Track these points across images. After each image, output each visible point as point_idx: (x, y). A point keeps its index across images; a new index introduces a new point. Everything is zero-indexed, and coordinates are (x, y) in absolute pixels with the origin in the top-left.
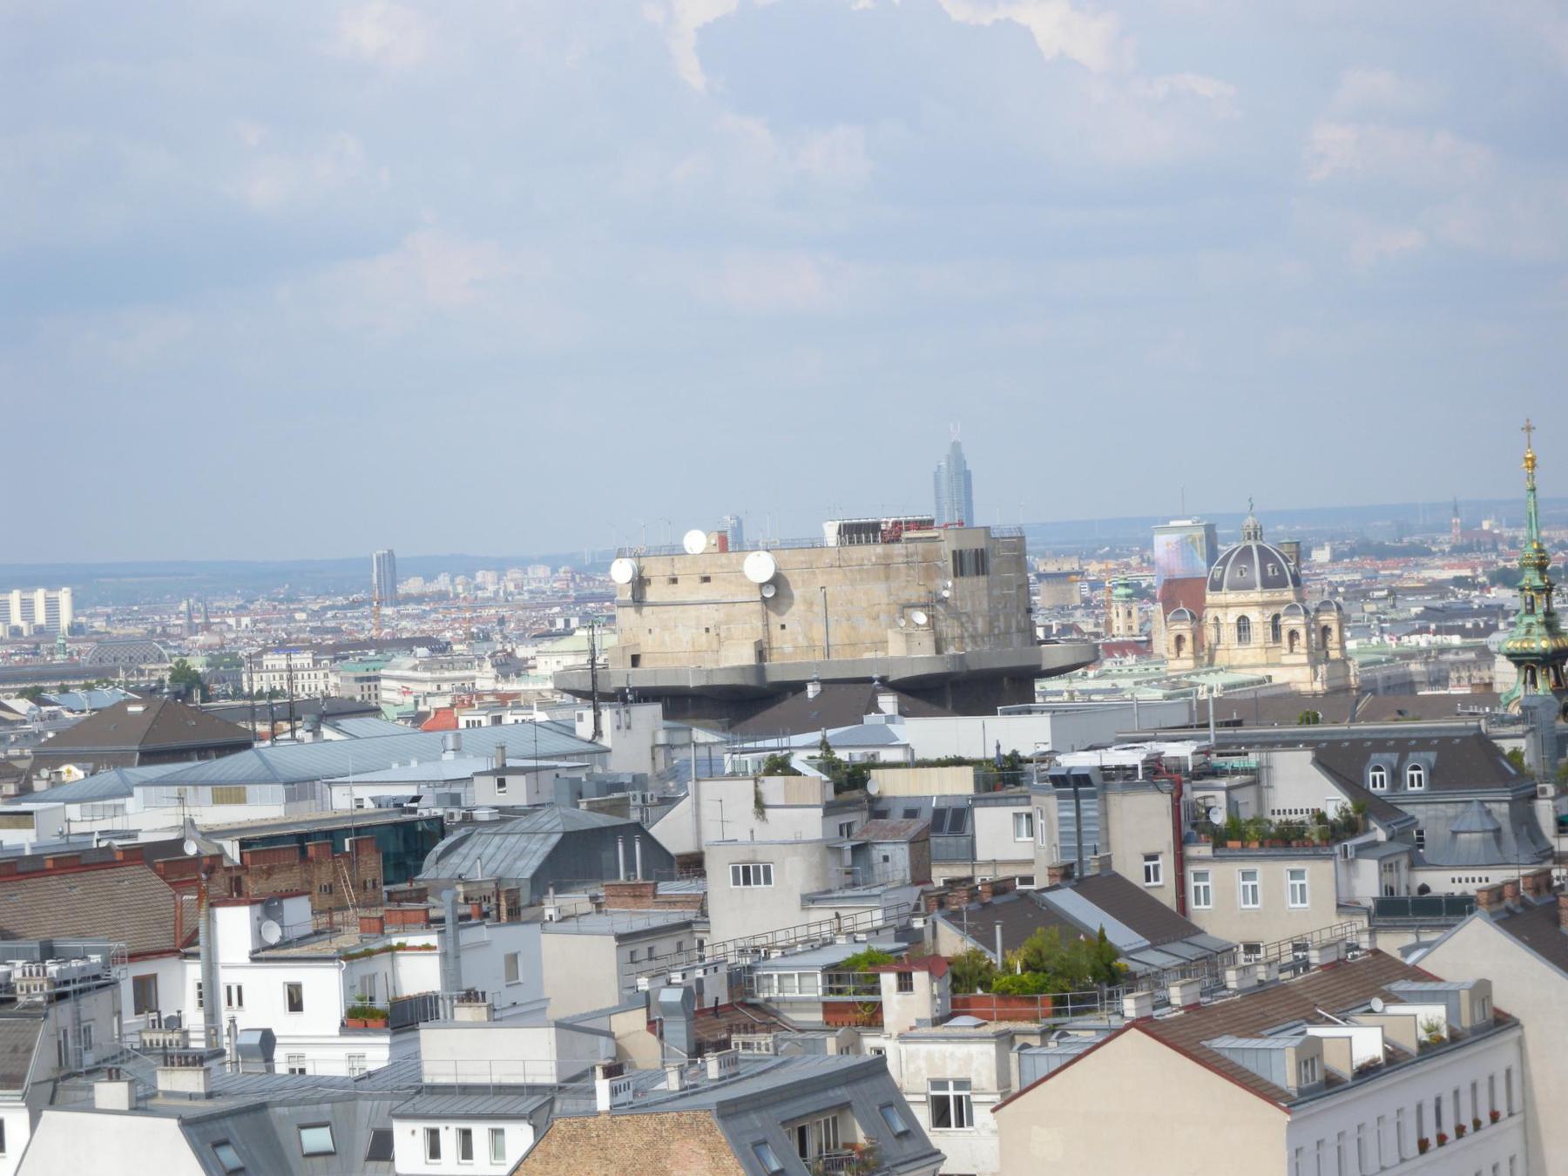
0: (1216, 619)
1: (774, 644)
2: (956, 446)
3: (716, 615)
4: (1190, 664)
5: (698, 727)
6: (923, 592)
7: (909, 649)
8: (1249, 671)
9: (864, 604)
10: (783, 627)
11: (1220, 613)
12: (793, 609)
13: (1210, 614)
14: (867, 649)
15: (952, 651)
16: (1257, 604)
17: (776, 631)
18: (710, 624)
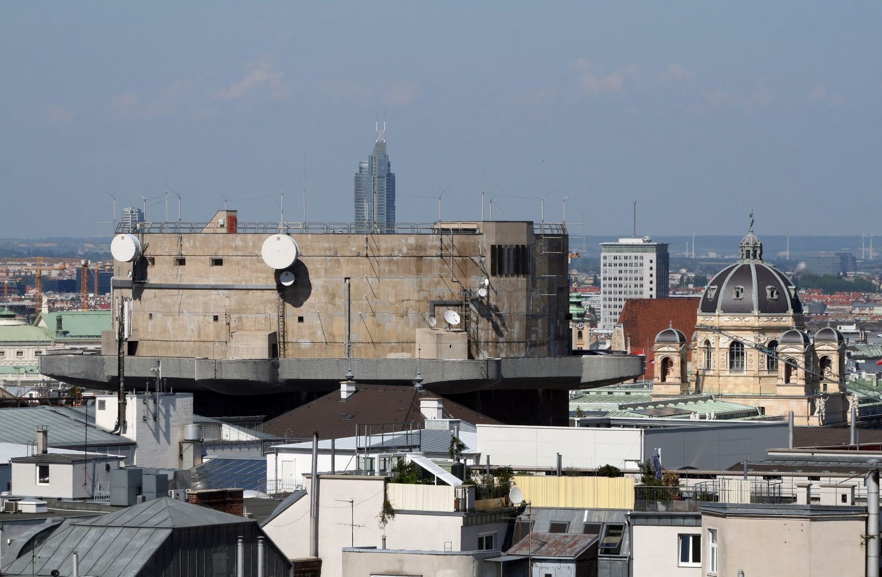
0: (707, 342)
1: (289, 338)
2: (380, 147)
3: (227, 302)
4: (676, 389)
5: (229, 422)
6: (456, 289)
7: (439, 351)
8: (740, 401)
9: (392, 299)
10: (301, 319)
11: (711, 337)
12: (311, 299)
13: (700, 337)
14: (392, 350)
15: (484, 355)
16: (753, 329)
17: (292, 322)
18: (220, 313)
